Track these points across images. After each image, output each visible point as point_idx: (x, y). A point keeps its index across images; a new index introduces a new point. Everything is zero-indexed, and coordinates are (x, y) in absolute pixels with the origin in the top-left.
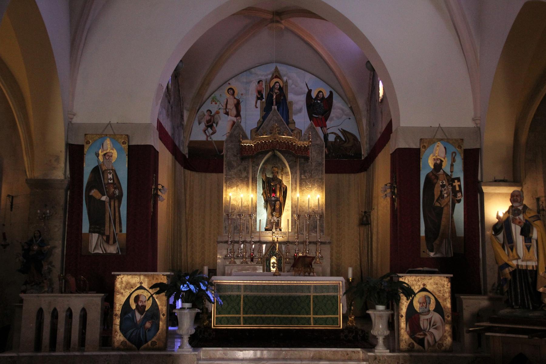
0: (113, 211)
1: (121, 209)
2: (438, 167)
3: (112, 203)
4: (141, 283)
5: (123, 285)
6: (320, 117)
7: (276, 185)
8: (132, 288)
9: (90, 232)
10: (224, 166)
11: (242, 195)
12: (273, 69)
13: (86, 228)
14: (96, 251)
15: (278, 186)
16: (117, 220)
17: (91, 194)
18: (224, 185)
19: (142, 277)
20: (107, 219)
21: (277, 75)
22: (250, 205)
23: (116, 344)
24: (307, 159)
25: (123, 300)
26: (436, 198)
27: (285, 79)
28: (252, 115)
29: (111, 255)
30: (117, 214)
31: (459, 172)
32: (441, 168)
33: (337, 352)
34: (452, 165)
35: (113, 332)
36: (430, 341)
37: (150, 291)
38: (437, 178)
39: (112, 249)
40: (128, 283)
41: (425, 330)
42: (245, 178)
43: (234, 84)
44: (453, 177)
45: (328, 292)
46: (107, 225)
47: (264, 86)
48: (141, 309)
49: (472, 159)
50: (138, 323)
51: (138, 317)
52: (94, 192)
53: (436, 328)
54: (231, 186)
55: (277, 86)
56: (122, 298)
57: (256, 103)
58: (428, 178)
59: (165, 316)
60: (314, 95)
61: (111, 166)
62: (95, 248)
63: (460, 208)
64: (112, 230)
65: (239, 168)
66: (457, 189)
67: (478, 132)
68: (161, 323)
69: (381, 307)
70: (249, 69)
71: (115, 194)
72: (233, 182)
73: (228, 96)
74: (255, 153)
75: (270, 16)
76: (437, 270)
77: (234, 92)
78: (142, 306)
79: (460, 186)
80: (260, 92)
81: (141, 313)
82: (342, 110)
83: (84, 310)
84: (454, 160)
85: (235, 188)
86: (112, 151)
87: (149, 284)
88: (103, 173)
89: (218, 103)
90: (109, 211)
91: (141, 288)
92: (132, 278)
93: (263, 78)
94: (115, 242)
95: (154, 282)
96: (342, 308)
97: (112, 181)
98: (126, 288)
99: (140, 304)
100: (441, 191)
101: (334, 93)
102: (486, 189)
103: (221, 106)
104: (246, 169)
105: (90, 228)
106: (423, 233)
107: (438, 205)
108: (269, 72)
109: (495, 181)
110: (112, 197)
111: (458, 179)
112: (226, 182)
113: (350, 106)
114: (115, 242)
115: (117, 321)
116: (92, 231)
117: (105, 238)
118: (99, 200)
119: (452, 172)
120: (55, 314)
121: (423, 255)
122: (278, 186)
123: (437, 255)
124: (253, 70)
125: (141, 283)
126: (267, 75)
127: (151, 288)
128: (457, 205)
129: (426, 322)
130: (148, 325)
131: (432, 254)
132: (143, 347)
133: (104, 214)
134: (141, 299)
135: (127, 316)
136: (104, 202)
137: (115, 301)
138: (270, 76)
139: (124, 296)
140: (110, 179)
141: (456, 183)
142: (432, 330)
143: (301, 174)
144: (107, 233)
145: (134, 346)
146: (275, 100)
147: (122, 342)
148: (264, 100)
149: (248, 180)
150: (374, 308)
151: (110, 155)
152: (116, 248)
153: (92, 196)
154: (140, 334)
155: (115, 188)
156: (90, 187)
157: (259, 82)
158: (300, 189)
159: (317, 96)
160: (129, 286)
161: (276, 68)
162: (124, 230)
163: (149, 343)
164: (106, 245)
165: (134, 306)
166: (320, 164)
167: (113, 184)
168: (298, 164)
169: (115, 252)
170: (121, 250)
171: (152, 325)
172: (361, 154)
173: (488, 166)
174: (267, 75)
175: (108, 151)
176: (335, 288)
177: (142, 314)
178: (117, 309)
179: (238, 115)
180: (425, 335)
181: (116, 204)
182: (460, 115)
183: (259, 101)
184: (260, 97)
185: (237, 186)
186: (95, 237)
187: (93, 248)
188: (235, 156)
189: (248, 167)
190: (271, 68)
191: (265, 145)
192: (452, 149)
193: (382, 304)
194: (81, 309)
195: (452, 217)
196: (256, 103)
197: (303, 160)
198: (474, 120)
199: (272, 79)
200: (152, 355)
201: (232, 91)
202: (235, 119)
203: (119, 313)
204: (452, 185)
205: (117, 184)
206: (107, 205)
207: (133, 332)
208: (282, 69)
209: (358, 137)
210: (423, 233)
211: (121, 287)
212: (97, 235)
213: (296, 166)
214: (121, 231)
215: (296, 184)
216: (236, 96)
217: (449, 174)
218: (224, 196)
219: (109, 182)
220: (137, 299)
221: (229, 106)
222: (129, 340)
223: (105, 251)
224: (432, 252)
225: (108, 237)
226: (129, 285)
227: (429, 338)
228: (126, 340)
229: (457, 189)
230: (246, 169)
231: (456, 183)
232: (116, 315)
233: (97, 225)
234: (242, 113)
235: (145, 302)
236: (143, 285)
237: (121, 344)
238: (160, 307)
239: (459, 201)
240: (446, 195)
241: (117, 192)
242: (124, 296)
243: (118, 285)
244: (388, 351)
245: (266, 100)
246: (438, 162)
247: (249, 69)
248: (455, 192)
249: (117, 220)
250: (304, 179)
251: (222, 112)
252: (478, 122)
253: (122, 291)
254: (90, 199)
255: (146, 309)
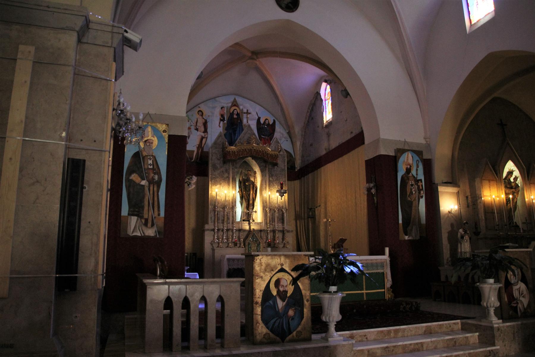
0: (152, 196)
1: (160, 193)
2: (408, 171)
3: (151, 188)
4: (282, 265)
5: (263, 267)
6: (267, 137)
7: (250, 185)
8: (272, 270)
9: (129, 214)
10: (210, 168)
11: (223, 192)
12: (232, 100)
13: (125, 210)
14: (134, 234)
15: (252, 186)
16: (156, 203)
17: (131, 178)
18: (210, 183)
19: (283, 259)
20: (146, 203)
21: (235, 104)
22: (231, 200)
23: (259, 338)
24: (276, 164)
25: (263, 285)
26: (408, 194)
27: (241, 107)
28: (216, 129)
29: (149, 238)
30: (156, 199)
31: (421, 176)
32: (410, 172)
33: (443, 325)
34: (417, 170)
35: (255, 324)
36: (521, 308)
37: (293, 273)
38: (408, 179)
39: (150, 232)
40: (268, 265)
41: (517, 299)
42: (226, 179)
43: (203, 107)
44: (418, 179)
45: (377, 269)
46: (146, 208)
47: (225, 111)
48: (282, 295)
49: (428, 165)
50: (280, 311)
51: (280, 304)
52: (134, 177)
53: (523, 297)
54: (215, 184)
55: (235, 112)
56: (262, 282)
57: (220, 123)
58: (402, 178)
59: (309, 302)
60: (262, 121)
61: (151, 153)
62: (133, 232)
63: (422, 203)
64: (150, 214)
65: (221, 170)
66: (421, 188)
67: (428, 146)
68: (305, 310)
69: (491, 281)
70: (215, 98)
71: (154, 179)
72: (217, 181)
73: (198, 116)
74: (238, 157)
75: (250, 55)
76: (517, 245)
77: (203, 114)
78: (283, 291)
79: (422, 186)
80: (222, 116)
81: (283, 300)
82: (282, 134)
83: (220, 299)
84: (418, 167)
85: (218, 186)
86: (153, 138)
87: (289, 267)
88: (144, 158)
89: (190, 121)
90: (148, 196)
91: (282, 270)
92: (272, 258)
93: (225, 105)
94: (153, 225)
95: (296, 264)
96: (388, 283)
97: (151, 167)
98: (265, 270)
99: (281, 289)
100: (411, 189)
101: (276, 121)
102: (441, 189)
103: (192, 124)
104: (227, 171)
105: (129, 211)
106: (400, 221)
107: (409, 199)
108: (229, 101)
109: (445, 183)
110: (151, 182)
111: (421, 180)
112: (211, 180)
113: (287, 131)
114: (153, 225)
115: (258, 310)
116: (131, 214)
117: (143, 221)
118: (139, 184)
119: (417, 175)
120: (186, 303)
121: (401, 238)
122: (252, 186)
123: (410, 238)
124: (217, 99)
125: (282, 265)
126: (227, 104)
127: (294, 270)
128: (421, 200)
129: (517, 291)
130: (291, 313)
131: (406, 238)
132: (288, 339)
133: (144, 197)
134: (282, 283)
135: (267, 304)
136: (143, 186)
137: (254, 286)
138: (230, 105)
139: (264, 281)
140: (150, 165)
141: (420, 184)
142: (522, 299)
143: (269, 177)
144: (146, 216)
145: (278, 338)
146: (233, 124)
147: (264, 335)
148: (225, 122)
149: (229, 180)
150: (485, 283)
151: (151, 141)
152: (154, 231)
153: (132, 180)
154: (283, 322)
155: (155, 174)
156: (130, 172)
157: (222, 108)
158: (269, 188)
159: (265, 122)
160: (269, 268)
161: (235, 99)
162: (162, 214)
163: (295, 333)
164: (144, 228)
165: (274, 293)
166: (284, 170)
167: (153, 169)
168: (267, 169)
169: (153, 235)
170: (159, 232)
171: (295, 313)
172: (295, 168)
173: (439, 174)
174: (227, 104)
175: (149, 138)
176: (382, 265)
177: (283, 300)
178: (257, 296)
179: (206, 131)
180: (517, 303)
181: (155, 189)
182: (416, 137)
183: (222, 122)
184: (222, 119)
185: (220, 184)
186: (134, 220)
187: (132, 231)
188: (218, 159)
189: (229, 169)
190: (231, 99)
191: (245, 152)
192: (417, 158)
193: (490, 277)
194: (217, 297)
195: (418, 209)
196: (220, 123)
197: (270, 166)
198: (425, 138)
199: (231, 107)
200: (308, 348)
201: (201, 113)
202: (203, 134)
203: (260, 300)
204: (417, 185)
205: (156, 169)
206: (147, 189)
207: (275, 322)
208: (239, 100)
209: (293, 155)
210: (400, 221)
211: (260, 269)
212: (136, 218)
213: (266, 170)
214: (159, 215)
215: (266, 185)
216: (204, 117)
217: (416, 176)
218: (210, 192)
219: (149, 167)
220: (278, 283)
221: (198, 124)
222: (271, 331)
223: (143, 233)
224: (406, 235)
225: (146, 220)
226: (269, 267)
227: (520, 306)
228: (269, 332)
229: (421, 188)
230: (227, 171)
231: (420, 184)
232: (257, 303)
233: (136, 209)
234: (209, 130)
235: (286, 286)
236: (284, 267)
237: (264, 337)
238: (303, 292)
239: (422, 197)
240: (414, 192)
241: (156, 177)
242: (264, 281)
243: (257, 268)
244: (501, 321)
245: (227, 122)
246: (409, 167)
247: (215, 98)
248: (419, 190)
249: (156, 203)
250: (270, 178)
251: (193, 128)
252: (428, 140)
253: (262, 274)
254: (131, 183)
255: (288, 295)
